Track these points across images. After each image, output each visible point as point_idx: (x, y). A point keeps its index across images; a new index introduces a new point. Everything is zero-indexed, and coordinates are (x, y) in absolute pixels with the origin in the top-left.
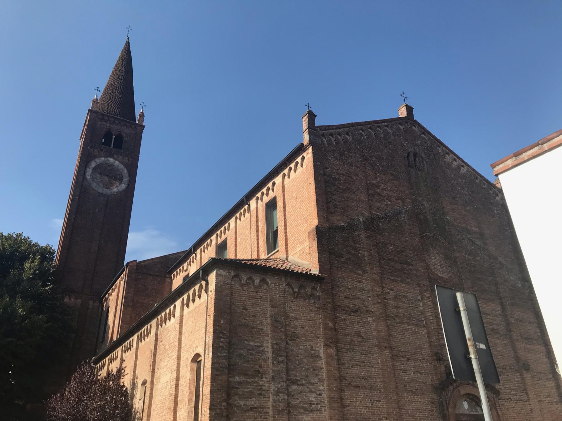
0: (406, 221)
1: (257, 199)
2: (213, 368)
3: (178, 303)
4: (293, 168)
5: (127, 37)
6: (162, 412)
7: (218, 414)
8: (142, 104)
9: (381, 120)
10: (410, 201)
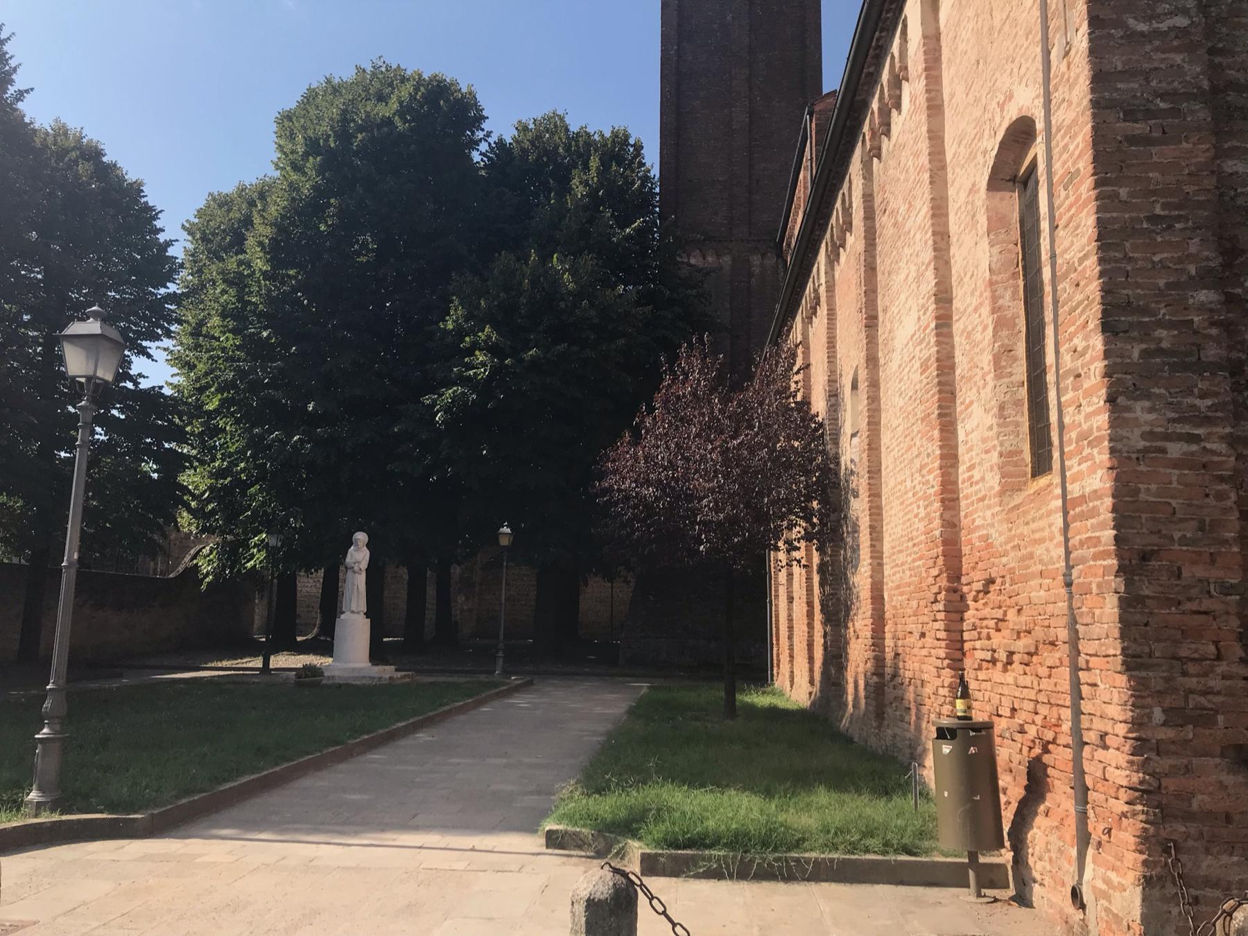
2: (1099, 106)
6: (910, 448)
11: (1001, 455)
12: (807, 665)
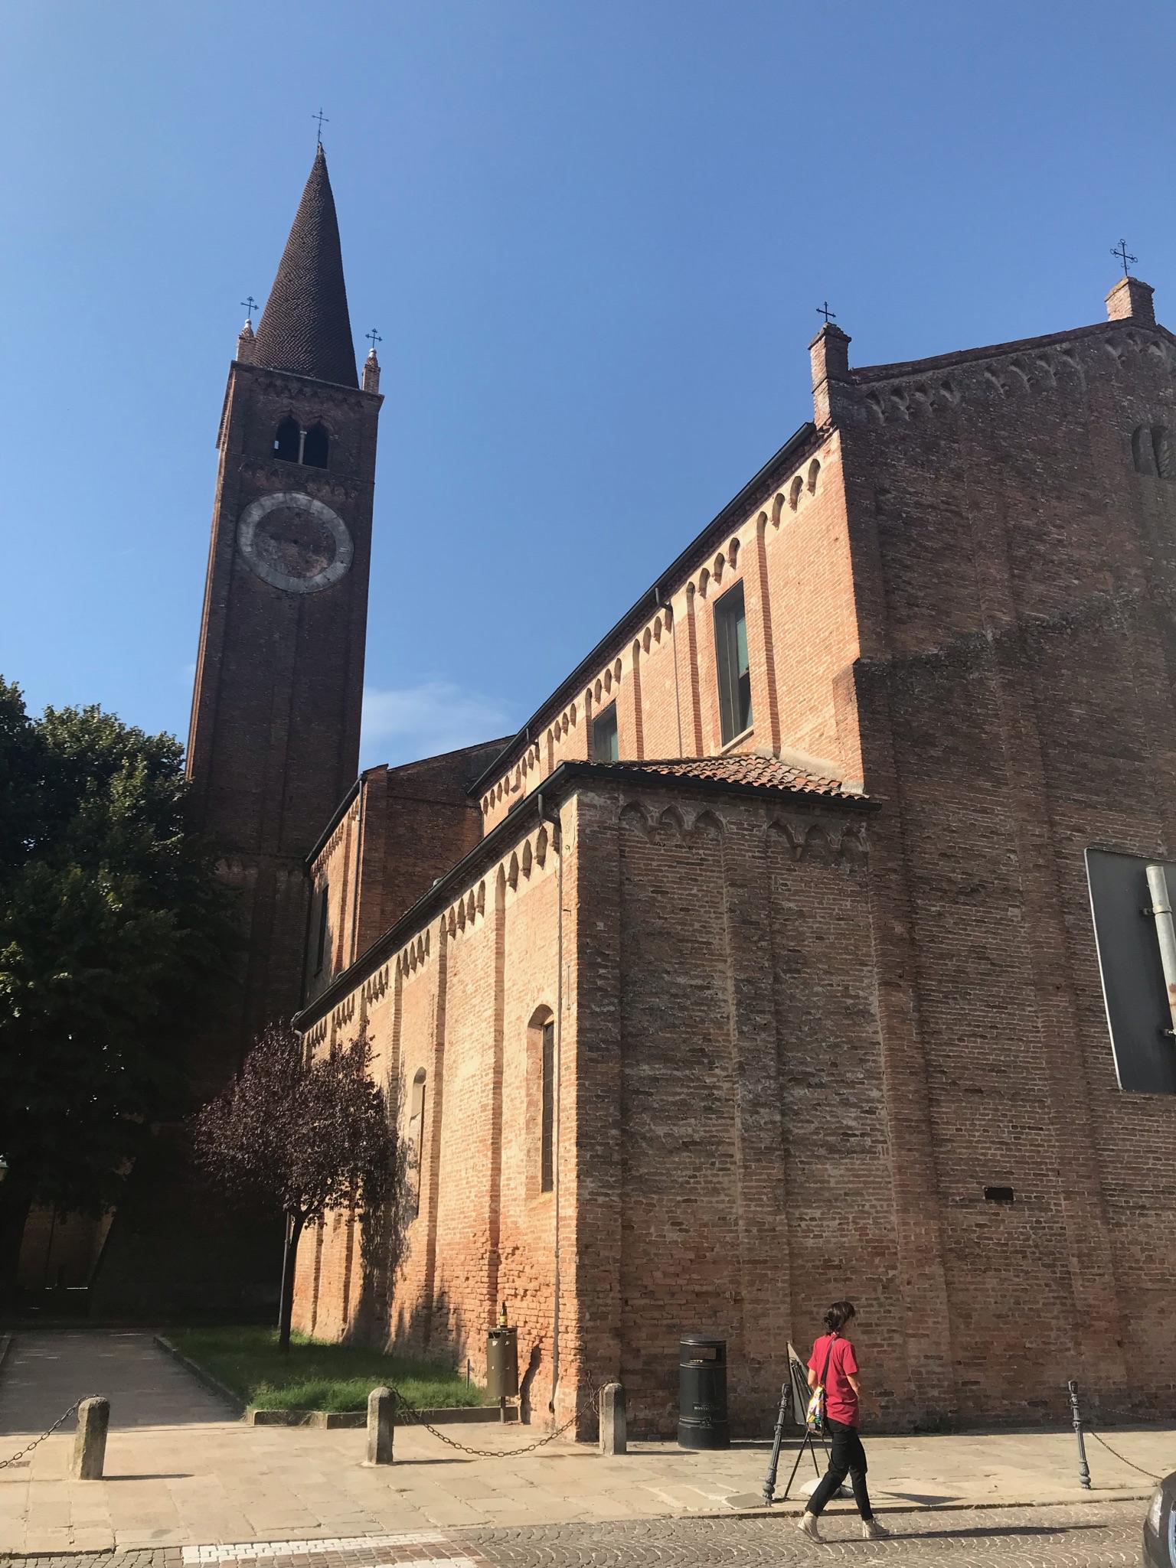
0: (1125, 631)
1: (691, 590)
3: (490, 877)
4: (787, 497)
5: (316, 144)
7: (602, 1157)
8: (372, 334)
9: (1050, 336)
10: (1138, 572)
11: (527, 1178)
12: (342, 1305)
